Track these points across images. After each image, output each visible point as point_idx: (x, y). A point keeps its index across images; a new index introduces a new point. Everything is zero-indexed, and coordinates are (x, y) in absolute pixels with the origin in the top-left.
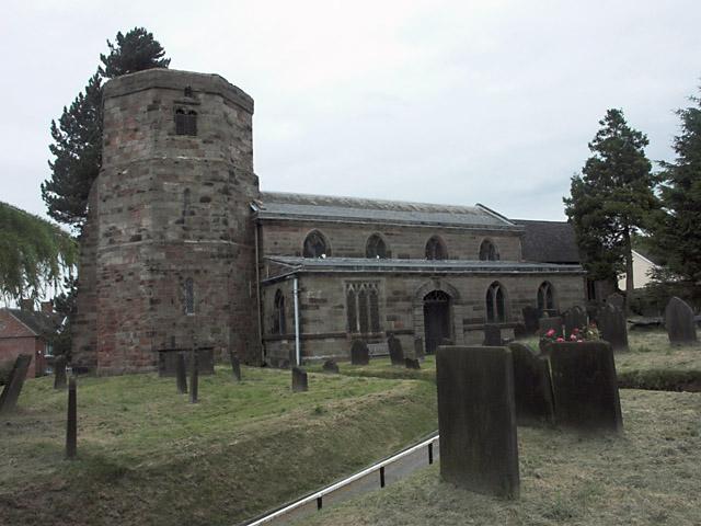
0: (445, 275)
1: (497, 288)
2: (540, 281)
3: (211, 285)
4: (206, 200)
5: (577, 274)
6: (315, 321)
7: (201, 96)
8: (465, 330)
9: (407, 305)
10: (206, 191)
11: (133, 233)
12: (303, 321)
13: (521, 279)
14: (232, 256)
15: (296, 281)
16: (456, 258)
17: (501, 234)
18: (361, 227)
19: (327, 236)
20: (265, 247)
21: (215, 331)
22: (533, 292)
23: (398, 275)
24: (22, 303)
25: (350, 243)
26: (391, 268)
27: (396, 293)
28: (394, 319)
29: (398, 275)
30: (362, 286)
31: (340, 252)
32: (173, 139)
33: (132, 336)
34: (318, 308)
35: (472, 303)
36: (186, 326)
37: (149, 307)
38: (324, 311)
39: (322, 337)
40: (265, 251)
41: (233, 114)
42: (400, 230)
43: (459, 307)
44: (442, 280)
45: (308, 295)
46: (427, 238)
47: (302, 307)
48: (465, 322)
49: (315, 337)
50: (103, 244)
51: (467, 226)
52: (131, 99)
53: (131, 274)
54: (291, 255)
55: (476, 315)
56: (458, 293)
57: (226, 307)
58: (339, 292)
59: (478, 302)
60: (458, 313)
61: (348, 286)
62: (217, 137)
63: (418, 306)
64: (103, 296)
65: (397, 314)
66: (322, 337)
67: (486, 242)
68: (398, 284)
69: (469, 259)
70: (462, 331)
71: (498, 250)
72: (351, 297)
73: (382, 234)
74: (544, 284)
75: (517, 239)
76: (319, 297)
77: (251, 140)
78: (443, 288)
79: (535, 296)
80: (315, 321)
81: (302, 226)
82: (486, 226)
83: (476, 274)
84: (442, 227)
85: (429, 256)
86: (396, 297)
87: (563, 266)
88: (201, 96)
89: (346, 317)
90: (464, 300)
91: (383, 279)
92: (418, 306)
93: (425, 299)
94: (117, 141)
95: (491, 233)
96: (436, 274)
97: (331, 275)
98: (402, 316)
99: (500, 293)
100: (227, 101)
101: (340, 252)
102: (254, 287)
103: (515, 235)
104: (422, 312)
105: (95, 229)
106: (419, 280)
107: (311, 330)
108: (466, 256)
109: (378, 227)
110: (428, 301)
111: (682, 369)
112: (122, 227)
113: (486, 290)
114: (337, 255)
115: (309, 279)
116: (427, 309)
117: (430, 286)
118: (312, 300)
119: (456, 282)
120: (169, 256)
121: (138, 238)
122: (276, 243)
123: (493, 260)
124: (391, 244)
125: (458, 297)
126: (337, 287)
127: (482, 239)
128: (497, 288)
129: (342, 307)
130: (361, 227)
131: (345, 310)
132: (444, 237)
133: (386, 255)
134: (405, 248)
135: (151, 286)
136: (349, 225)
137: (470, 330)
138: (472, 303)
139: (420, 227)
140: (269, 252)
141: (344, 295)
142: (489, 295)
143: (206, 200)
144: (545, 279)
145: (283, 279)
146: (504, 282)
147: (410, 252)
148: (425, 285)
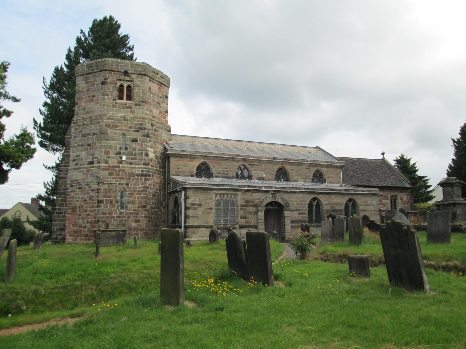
0: (279, 192)
1: (316, 202)
2: (346, 198)
3: (136, 193)
4: (135, 141)
5: (374, 195)
6: (193, 217)
7: (134, 76)
8: (292, 227)
9: (253, 209)
10: (135, 135)
11: (91, 160)
12: (186, 217)
13: (333, 196)
14: (150, 175)
15: (183, 192)
16: (296, 181)
17: (328, 166)
18: (234, 160)
19: (211, 165)
20: (171, 170)
21: (137, 221)
22: (342, 204)
23: (248, 191)
24: (357, 217)
25: (226, 170)
26: (245, 186)
27: (247, 202)
28: (245, 218)
29: (248, 191)
30: (226, 196)
31: (218, 175)
32: (116, 103)
33: (86, 222)
34: (195, 209)
35: (297, 210)
36: (119, 217)
37: (96, 204)
38: (199, 211)
39: (198, 227)
40: (171, 173)
41: (155, 87)
42: (258, 162)
43: (289, 212)
44: (277, 195)
45: (190, 201)
46: (277, 167)
47: (186, 208)
48: (292, 222)
49: (192, 227)
50: (72, 165)
51: (304, 160)
52: (91, 78)
53: (87, 185)
54: (188, 176)
55: (300, 218)
56: (288, 203)
57: (144, 207)
58: (212, 199)
59: (301, 210)
60: (288, 216)
61: (216, 196)
62: (143, 102)
63: (261, 211)
64: (70, 198)
65: (247, 215)
66: (198, 227)
67: (317, 171)
68: (249, 196)
69: (305, 182)
70: (290, 227)
71: (326, 177)
72: (218, 204)
73: (247, 164)
74: (350, 200)
75: (339, 170)
76: (197, 202)
77: (167, 104)
78: (279, 200)
79: (343, 208)
80: (193, 217)
81: (195, 158)
82: (317, 161)
83: (301, 192)
84: (286, 161)
85: (278, 178)
86: (247, 204)
87: (365, 189)
88: (134, 76)
89: (214, 215)
90: (292, 208)
91: (239, 193)
92: (261, 211)
93: (266, 206)
94: (83, 104)
95: (321, 166)
96: (274, 191)
97: (205, 189)
98: (250, 216)
99: (318, 206)
100: (152, 79)
101: (218, 175)
102: (164, 195)
103: (337, 167)
104: (263, 214)
105: (68, 156)
106: (262, 194)
107: (190, 222)
108: (302, 180)
109: (244, 160)
110: (269, 207)
111: (355, 256)
112: (83, 154)
113: (308, 202)
114: (217, 177)
115: (191, 191)
116: (267, 212)
117: (269, 198)
118: (193, 204)
119: (286, 196)
120: (111, 174)
121: (92, 163)
122: (178, 169)
123: (322, 183)
124: (215, 168)
125: (288, 206)
126: (209, 197)
127: (315, 169)
128: (316, 202)
129: (211, 209)
130: (234, 160)
131: (214, 211)
132: (288, 167)
133: (210, 175)
134: (261, 174)
135: (98, 192)
136: (226, 159)
137: (295, 227)
138: (297, 210)
139: (273, 161)
140: (174, 173)
141: (214, 203)
142: (310, 205)
143: (135, 141)
144: (351, 197)
145: (176, 191)
146: (321, 198)
147: (264, 176)
148: (266, 198)
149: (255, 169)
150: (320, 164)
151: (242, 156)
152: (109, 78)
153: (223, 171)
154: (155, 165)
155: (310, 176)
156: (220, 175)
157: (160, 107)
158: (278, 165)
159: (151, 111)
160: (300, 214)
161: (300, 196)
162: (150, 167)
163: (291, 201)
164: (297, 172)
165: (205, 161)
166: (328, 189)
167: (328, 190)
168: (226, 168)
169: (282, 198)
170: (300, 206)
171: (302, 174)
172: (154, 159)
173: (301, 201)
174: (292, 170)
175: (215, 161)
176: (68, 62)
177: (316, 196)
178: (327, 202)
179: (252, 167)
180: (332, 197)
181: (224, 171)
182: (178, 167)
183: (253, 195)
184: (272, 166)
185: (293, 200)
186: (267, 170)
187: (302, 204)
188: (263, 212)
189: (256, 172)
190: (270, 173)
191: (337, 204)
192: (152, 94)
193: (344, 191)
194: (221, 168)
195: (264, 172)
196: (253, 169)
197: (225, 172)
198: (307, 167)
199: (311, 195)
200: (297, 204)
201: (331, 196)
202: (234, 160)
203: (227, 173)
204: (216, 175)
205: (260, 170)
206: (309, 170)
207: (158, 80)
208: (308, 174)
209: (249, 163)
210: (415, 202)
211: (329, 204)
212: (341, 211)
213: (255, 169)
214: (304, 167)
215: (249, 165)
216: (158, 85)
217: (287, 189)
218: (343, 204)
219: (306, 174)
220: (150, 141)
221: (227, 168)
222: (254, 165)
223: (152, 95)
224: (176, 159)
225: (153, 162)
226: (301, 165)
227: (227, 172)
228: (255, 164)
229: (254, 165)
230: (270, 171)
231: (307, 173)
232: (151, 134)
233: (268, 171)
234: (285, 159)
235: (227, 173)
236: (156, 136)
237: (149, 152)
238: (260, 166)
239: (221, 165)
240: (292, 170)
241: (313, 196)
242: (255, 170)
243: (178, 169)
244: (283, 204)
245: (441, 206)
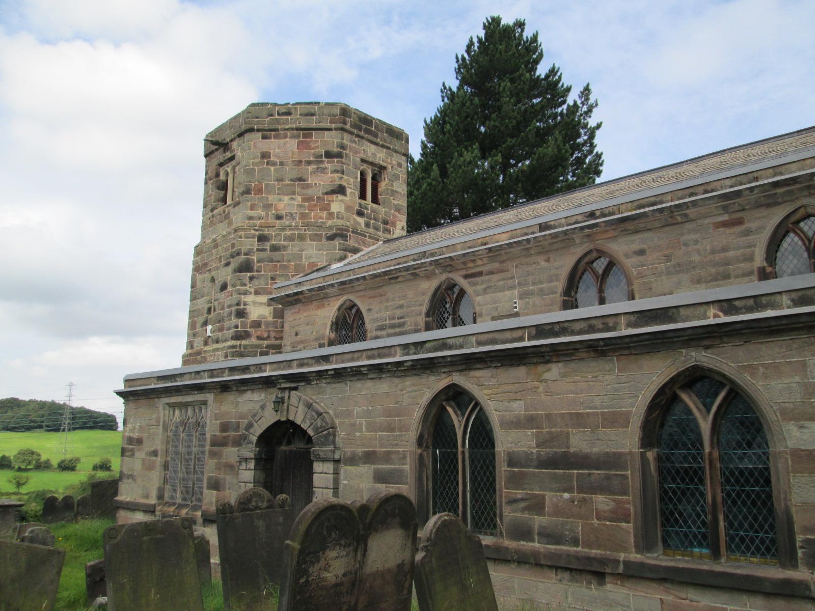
13: (554, 370)
22: (615, 420)
25: (398, 312)
31: (379, 333)
35: (369, 457)
51: (691, 191)
59: (387, 457)
122: (297, 334)
138: (369, 457)
149: (485, 289)
150: (794, 180)
151: (432, 255)
152: (468, 152)
153: (390, 319)
154: (273, 334)
155: (750, 258)
156: (384, 333)
157: (308, 186)
158: (572, 250)
159: (268, 207)
160: (380, 478)
161: (384, 386)
162: (253, 341)
163: (349, 414)
164: (668, 258)
165: (350, 297)
166: (518, 334)
167: (521, 339)
168: (398, 308)
169: (309, 406)
170: (381, 438)
171: (696, 258)
172: (270, 319)
173: (388, 413)
174: (641, 252)
175: (372, 293)
176: (424, 146)
177: (458, 379)
178: (518, 408)
179: (474, 284)
180: (547, 376)
181: (394, 318)
182: (297, 328)
183: (240, 399)
184: (548, 260)
185: (357, 410)
186: (530, 279)
187: (390, 429)
188: (252, 465)
189: (488, 297)
190: (541, 290)
191: (579, 420)
192: (274, 164)
193: (629, 325)
194: (387, 308)
195: (516, 292)
196: (480, 288)
197: (397, 321)
198: (726, 217)
199: (432, 378)
200: (372, 427)
201: (541, 368)
202: (415, 275)
203: (402, 320)
204: (375, 333)
205: (502, 290)
206: (738, 229)
207: (294, 126)
208: (731, 254)
209: (463, 272)
210: (731, 391)
211: (531, 421)
212: (612, 461)
213: (484, 286)
214: (707, 221)
215: (466, 277)
216: (292, 137)
217: (255, 372)
218: (627, 415)
219: (718, 257)
220: (251, 278)
221: (401, 307)
222: (480, 274)
223: (272, 168)
224: (293, 311)
225: (263, 327)
226: (687, 219)
227: (402, 318)
228: (484, 269)
229: (480, 274)
230: (541, 282)
231: (725, 250)
232: (258, 261)
233: (534, 284)
234: (592, 215)
235: (402, 320)
236: (278, 261)
237: (247, 307)
238: (502, 271)
239: (387, 300)
240: (641, 252)
241: (437, 383)
242: (485, 291)
243: (297, 334)
244: (311, 432)
245: (532, 561)
